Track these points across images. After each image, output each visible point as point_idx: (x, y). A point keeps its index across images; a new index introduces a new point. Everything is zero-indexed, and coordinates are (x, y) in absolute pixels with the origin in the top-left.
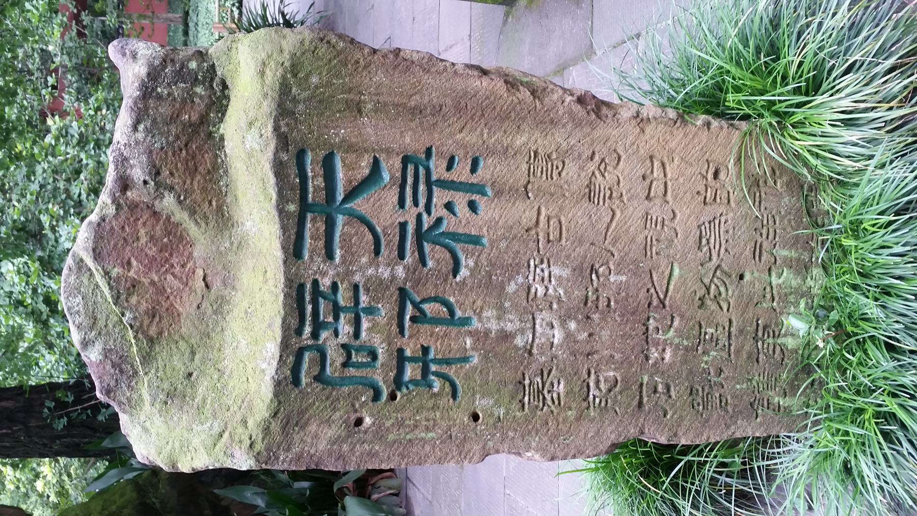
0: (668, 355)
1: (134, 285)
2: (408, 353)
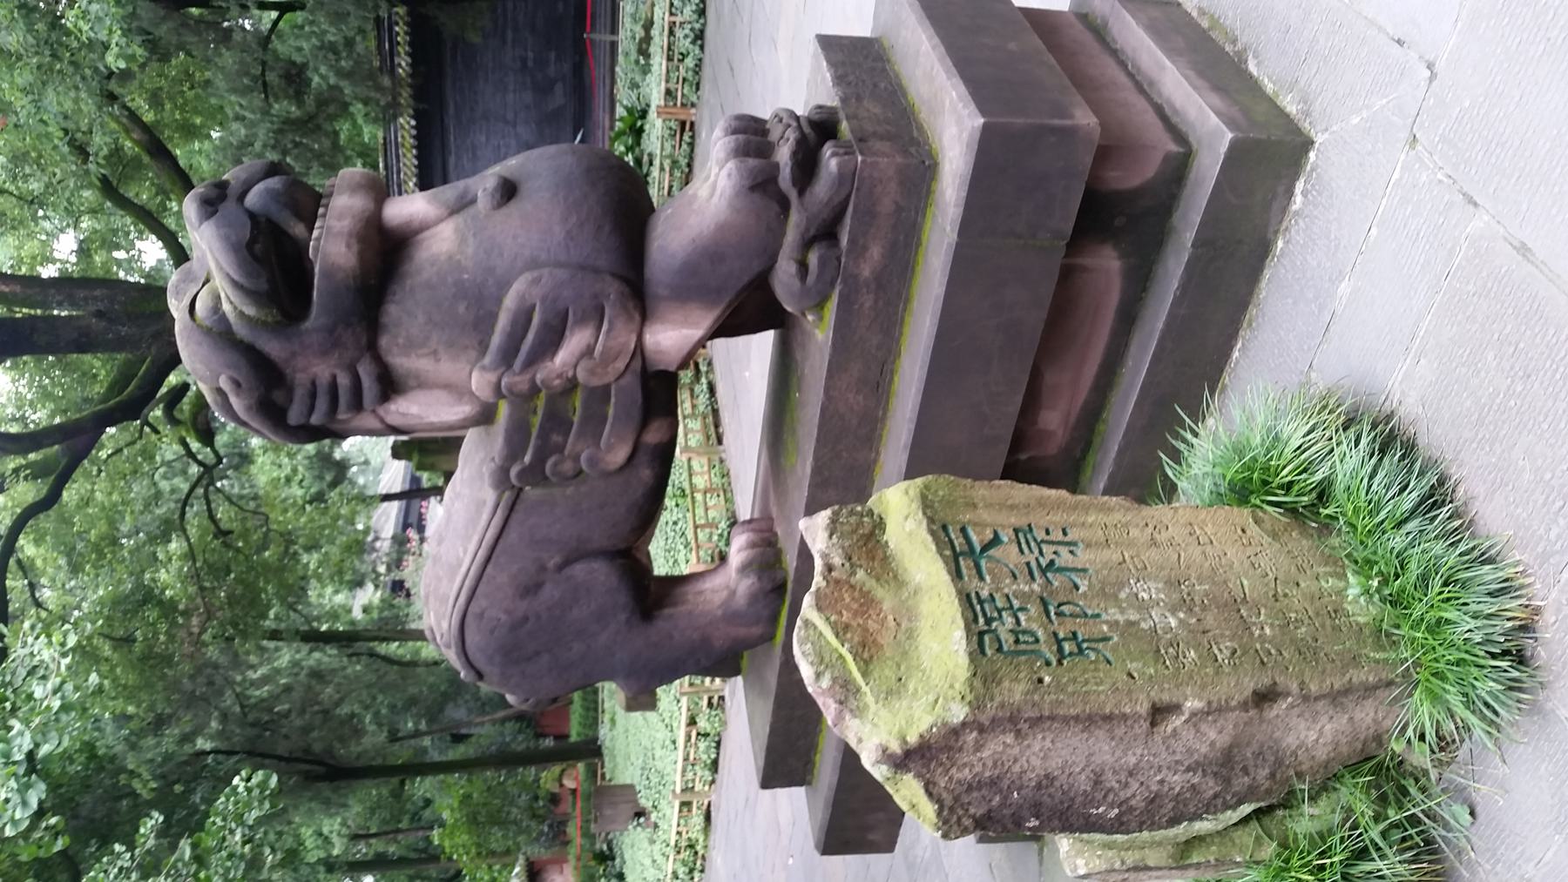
0: (1268, 631)
1: (847, 627)
2: (1061, 635)
